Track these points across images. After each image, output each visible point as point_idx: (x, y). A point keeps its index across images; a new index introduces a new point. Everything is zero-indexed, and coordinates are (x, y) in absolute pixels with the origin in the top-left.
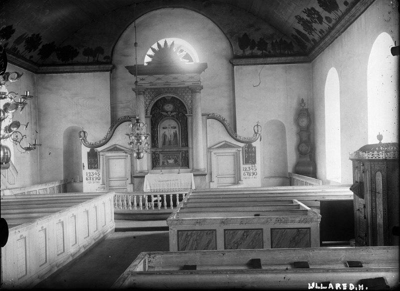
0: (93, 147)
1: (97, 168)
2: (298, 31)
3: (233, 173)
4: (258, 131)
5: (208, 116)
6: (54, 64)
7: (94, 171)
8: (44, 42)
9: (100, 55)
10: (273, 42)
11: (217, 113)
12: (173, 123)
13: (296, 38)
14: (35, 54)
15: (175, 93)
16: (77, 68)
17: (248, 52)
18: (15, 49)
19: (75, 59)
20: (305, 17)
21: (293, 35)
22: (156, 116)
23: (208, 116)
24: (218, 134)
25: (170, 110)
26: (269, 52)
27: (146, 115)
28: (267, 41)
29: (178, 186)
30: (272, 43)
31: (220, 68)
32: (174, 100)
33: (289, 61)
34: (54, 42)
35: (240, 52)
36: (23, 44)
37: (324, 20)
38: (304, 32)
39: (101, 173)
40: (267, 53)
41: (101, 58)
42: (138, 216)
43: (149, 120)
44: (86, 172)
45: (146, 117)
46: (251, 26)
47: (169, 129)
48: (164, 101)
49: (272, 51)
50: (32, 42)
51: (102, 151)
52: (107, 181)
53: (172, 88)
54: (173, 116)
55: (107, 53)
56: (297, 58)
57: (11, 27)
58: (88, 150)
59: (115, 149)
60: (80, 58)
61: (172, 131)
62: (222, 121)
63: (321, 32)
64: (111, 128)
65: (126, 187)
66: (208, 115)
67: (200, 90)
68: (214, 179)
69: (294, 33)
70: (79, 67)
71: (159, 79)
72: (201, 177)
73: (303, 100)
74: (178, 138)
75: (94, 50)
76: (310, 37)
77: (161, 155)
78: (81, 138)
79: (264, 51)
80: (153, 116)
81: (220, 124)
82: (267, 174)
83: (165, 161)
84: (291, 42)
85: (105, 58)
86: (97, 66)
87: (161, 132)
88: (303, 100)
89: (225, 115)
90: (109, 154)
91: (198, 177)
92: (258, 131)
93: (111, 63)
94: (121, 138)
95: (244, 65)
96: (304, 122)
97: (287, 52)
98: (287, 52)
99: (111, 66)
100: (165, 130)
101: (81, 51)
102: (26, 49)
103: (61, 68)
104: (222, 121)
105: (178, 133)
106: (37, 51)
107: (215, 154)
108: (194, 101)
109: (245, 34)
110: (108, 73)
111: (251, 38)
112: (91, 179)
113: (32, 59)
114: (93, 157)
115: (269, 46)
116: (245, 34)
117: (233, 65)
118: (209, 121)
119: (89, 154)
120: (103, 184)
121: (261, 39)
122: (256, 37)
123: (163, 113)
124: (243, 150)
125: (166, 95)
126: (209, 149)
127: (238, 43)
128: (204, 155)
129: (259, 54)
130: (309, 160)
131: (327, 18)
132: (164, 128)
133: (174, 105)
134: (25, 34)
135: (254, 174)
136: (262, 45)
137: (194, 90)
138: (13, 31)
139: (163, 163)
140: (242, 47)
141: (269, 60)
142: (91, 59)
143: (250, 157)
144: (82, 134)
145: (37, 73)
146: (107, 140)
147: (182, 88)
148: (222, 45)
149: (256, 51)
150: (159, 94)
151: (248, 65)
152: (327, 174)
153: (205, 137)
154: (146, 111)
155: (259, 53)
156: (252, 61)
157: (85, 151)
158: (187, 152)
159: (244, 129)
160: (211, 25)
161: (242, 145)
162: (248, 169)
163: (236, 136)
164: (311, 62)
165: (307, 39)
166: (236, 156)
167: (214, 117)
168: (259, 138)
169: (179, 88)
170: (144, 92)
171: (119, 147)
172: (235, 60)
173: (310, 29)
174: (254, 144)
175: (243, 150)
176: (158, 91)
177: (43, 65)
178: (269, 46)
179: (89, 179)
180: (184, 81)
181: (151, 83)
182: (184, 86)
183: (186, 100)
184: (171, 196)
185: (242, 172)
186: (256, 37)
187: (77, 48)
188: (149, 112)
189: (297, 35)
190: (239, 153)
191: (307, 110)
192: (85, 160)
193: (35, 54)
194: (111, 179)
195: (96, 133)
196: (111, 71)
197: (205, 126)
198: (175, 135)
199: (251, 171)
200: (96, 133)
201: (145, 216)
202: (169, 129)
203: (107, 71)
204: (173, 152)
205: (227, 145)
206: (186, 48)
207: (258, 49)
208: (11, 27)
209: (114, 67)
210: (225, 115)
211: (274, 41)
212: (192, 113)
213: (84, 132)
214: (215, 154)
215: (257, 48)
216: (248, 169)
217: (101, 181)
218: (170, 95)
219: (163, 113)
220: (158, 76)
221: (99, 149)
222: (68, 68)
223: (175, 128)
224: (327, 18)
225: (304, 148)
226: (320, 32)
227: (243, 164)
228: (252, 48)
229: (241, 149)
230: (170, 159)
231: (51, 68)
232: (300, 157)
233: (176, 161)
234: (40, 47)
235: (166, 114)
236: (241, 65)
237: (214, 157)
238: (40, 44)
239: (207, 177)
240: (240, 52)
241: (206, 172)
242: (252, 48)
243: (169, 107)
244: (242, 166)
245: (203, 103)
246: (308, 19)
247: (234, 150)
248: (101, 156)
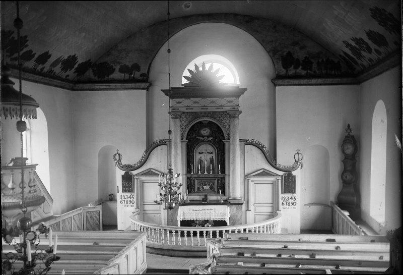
0: (129, 168)
1: (131, 191)
2: (345, 53)
3: (270, 201)
4: (299, 159)
5: (246, 142)
6: (90, 81)
7: (129, 194)
8: (80, 61)
9: (136, 72)
10: (319, 61)
11: (256, 139)
12: (210, 148)
13: (344, 59)
14: (71, 73)
15: (211, 117)
16: (113, 85)
17: (292, 72)
18: (51, 71)
19: (111, 76)
20: (353, 44)
21: (340, 56)
22: (192, 142)
23: (246, 142)
24: (257, 161)
25: (207, 134)
26: (315, 72)
27: (182, 139)
28: (313, 60)
29: (215, 216)
30: (318, 63)
31: (264, 84)
32: (210, 125)
33: (336, 82)
34: (90, 60)
35: (283, 72)
36: (60, 65)
37: (373, 51)
38: (352, 55)
39: (135, 197)
40: (312, 73)
41: (137, 75)
42: (171, 252)
43: (185, 145)
44: (120, 195)
45: (181, 142)
46: (295, 44)
47: (205, 154)
48: (201, 125)
49: (317, 72)
50: (69, 62)
51: (136, 175)
52: (141, 205)
53: (209, 113)
54: (210, 141)
55: (144, 70)
56: (345, 80)
57: (47, 53)
58: (123, 173)
59: (150, 173)
60: (117, 75)
61: (209, 156)
62: (261, 148)
63: (370, 60)
64: (146, 151)
65: (160, 212)
66: (247, 141)
67: (239, 114)
68: (251, 207)
69: (342, 54)
70: (115, 84)
71: (196, 102)
72: (237, 206)
73: (349, 126)
74: (215, 164)
75: (130, 66)
76: (359, 62)
77: (196, 181)
78: (116, 161)
79: (309, 71)
80: (189, 141)
81: (259, 151)
82: (307, 202)
83: (201, 187)
84: (339, 62)
85: (141, 75)
86: (133, 84)
87: (197, 157)
88: (349, 126)
89: (266, 144)
90: (143, 178)
91: (234, 206)
92: (299, 159)
93: (146, 81)
94: (157, 161)
95: (287, 85)
96: (350, 150)
97: (333, 72)
98: (333, 72)
99: (147, 84)
100: (201, 155)
101: (117, 68)
102: (62, 70)
103: (97, 86)
104: (261, 148)
105: (214, 159)
106: (73, 70)
107: (252, 181)
108: (232, 127)
109: (289, 52)
110: (145, 91)
111: (295, 56)
112: (126, 202)
113: (67, 78)
114: (128, 180)
115: (315, 66)
116: (289, 52)
117: (275, 86)
118: (247, 147)
119: (123, 177)
120: (138, 207)
121: (306, 58)
122: (300, 55)
123: (199, 138)
124: (282, 179)
125: (203, 119)
126: (247, 177)
127: (281, 62)
128: (241, 183)
129: (303, 74)
130: (353, 191)
131: (376, 50)
132: (200, 153)
133: (211, 130)
134: (61, 57)
135: (293, 204)
136: (307, 64)
137: (234, 114)
138: (50, 56)
139: (199, 189)
140: (286, 66)
141: (314, 81)
142: (127, 76)
143: (289, 184)
144: (117, 157)
145: (73, 89)
146: (142, 163)
147: (219, 112)
148: (264, 61)
149: (300, 71)
150: (199, 117)
151: (290, 85)
152: (371, 213)
153: (242, 164)
154: (182, 135)
155: (304, 73)
156: (296, 82)
157: (119, 173)
158: (224, 178)
159: (284, 158)
160: (252, 40)
161: (281, 173)
162: (286, 198)
163: (276, 165)
164: (359, 84)
165: (356, 63)
166: (274, 184)
167: (252, 144)
168: (300, 167)
169: (216, 112)
170: (180, 116)
171: (153, 171)
172: (278, 79)
173: (360, 56)
174: (294, 173)
175: (282, 179)
176: (195, 115)
177: (79, 82)
178: (315, 66)
179: (123, 202)
180: (221, 106)
181: (188, 106)
182: (222, 110)
183: (223, 124)
184: (205, 232)
185: (281, 202)
186: (300, 55)
187: (113, 65)
188: (185, 136)
189: (345, 56)
190: (278, 182)
191: (353, 137)
192: (119, 183)
193: (71, 73)
194: (145, 203)
195: (131, 156)
196: (147, 89)
197: (243, 152)
198: (212, 161)
199: (290, 201)
200: (131, 156)
201: (177, 252)
202: (205, 154)
203: (144, 89)
204: (209, 182)
205: (265, 173)
206: (222, 66)
207: (303, 69)
208: (47, 53)
209: (151, 85)
210: (266, 144)
211: (320, 61)
212: (229, 139)
213: (119, 155)
214: (252, 181)
215: (301, 67)
216: (286, 198)
217: (135, 205)
218: (207, 119)
219: (199, 138)
220: (195, 99)
221: (134, 172)
222: (104, 86)
223: (212, 153)
224: (376, 50)
225: (349, 177)
226: (369, 60)
227: (282, 193)
228: (296, 68)
229: (280, 178)
230: (205, 185)
231: (88, 86)
232: (343, 186)
233: (211, 188)
234: (76, 66)
235: (202, 139)
236: (284, 85)
237: (251, 184)
238: (76, 63)
239: (244, 206)
240: (283, 72)
241: (243, 200)
242: (296, 68)
243: (205, 132)
244: (281, 195)
245: (241, 128)
246: (357, 46)
247: (272, 179)
248: (136, 180)
